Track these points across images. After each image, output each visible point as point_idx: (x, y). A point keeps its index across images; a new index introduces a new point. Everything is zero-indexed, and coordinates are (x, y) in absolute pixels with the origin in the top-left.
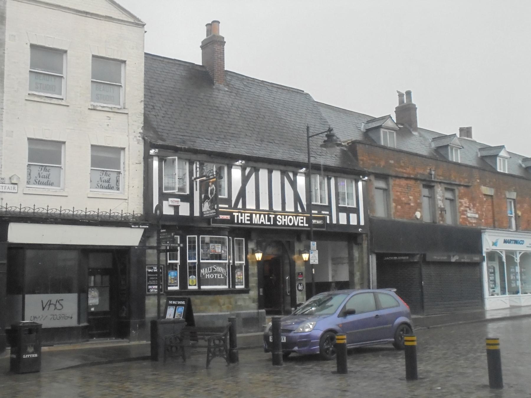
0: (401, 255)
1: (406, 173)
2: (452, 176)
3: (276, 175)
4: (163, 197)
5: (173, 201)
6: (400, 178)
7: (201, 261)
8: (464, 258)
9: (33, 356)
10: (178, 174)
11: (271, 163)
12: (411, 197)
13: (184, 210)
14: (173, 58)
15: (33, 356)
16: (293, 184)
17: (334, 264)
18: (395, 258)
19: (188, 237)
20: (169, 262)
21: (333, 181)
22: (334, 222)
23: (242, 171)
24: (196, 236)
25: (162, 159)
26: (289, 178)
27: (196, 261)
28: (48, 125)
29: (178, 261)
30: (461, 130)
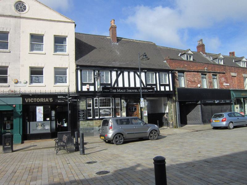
0: (192, 101)
1: (193, 69)
2: (216, 69)
3: (132, 74)
4: (83, 84)
5: (87, 86)
6: (191, 71)
7: (100, 107)
8: (222, 101)
9: (9, 146)
10: (90, 76)
11: (129, 69)
12: (196, 79)
13: (92, 89)
14: (241, 57)
15: (9, 146)
16: (139, 77)
17: (164, 106)
18: (190, 103)
19: (95, 99)
20: (116, 107)
21: (157, 74)
22: (159, 90)
23: (116, 73)
24: (97, 98)
25: (81, 71)
26: (137, 74)
27: (98, 107)
28: (36, 60)
29: (91, 108)
30: (230, 53)
